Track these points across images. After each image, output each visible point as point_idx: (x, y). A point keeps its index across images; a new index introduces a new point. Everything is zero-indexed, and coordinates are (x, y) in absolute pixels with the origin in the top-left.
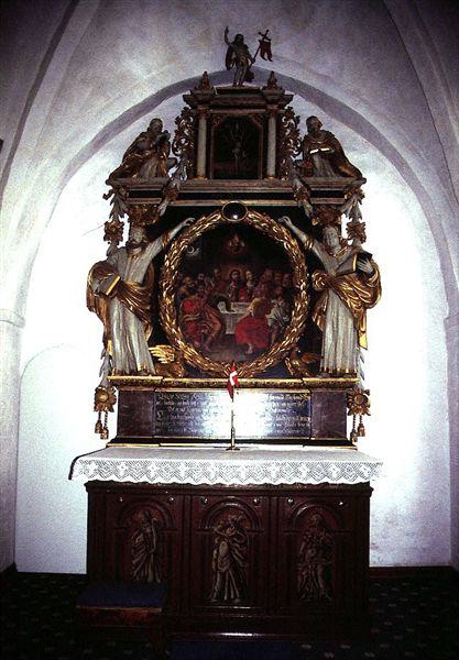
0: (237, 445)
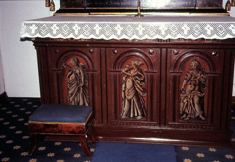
0: (142, 13)
